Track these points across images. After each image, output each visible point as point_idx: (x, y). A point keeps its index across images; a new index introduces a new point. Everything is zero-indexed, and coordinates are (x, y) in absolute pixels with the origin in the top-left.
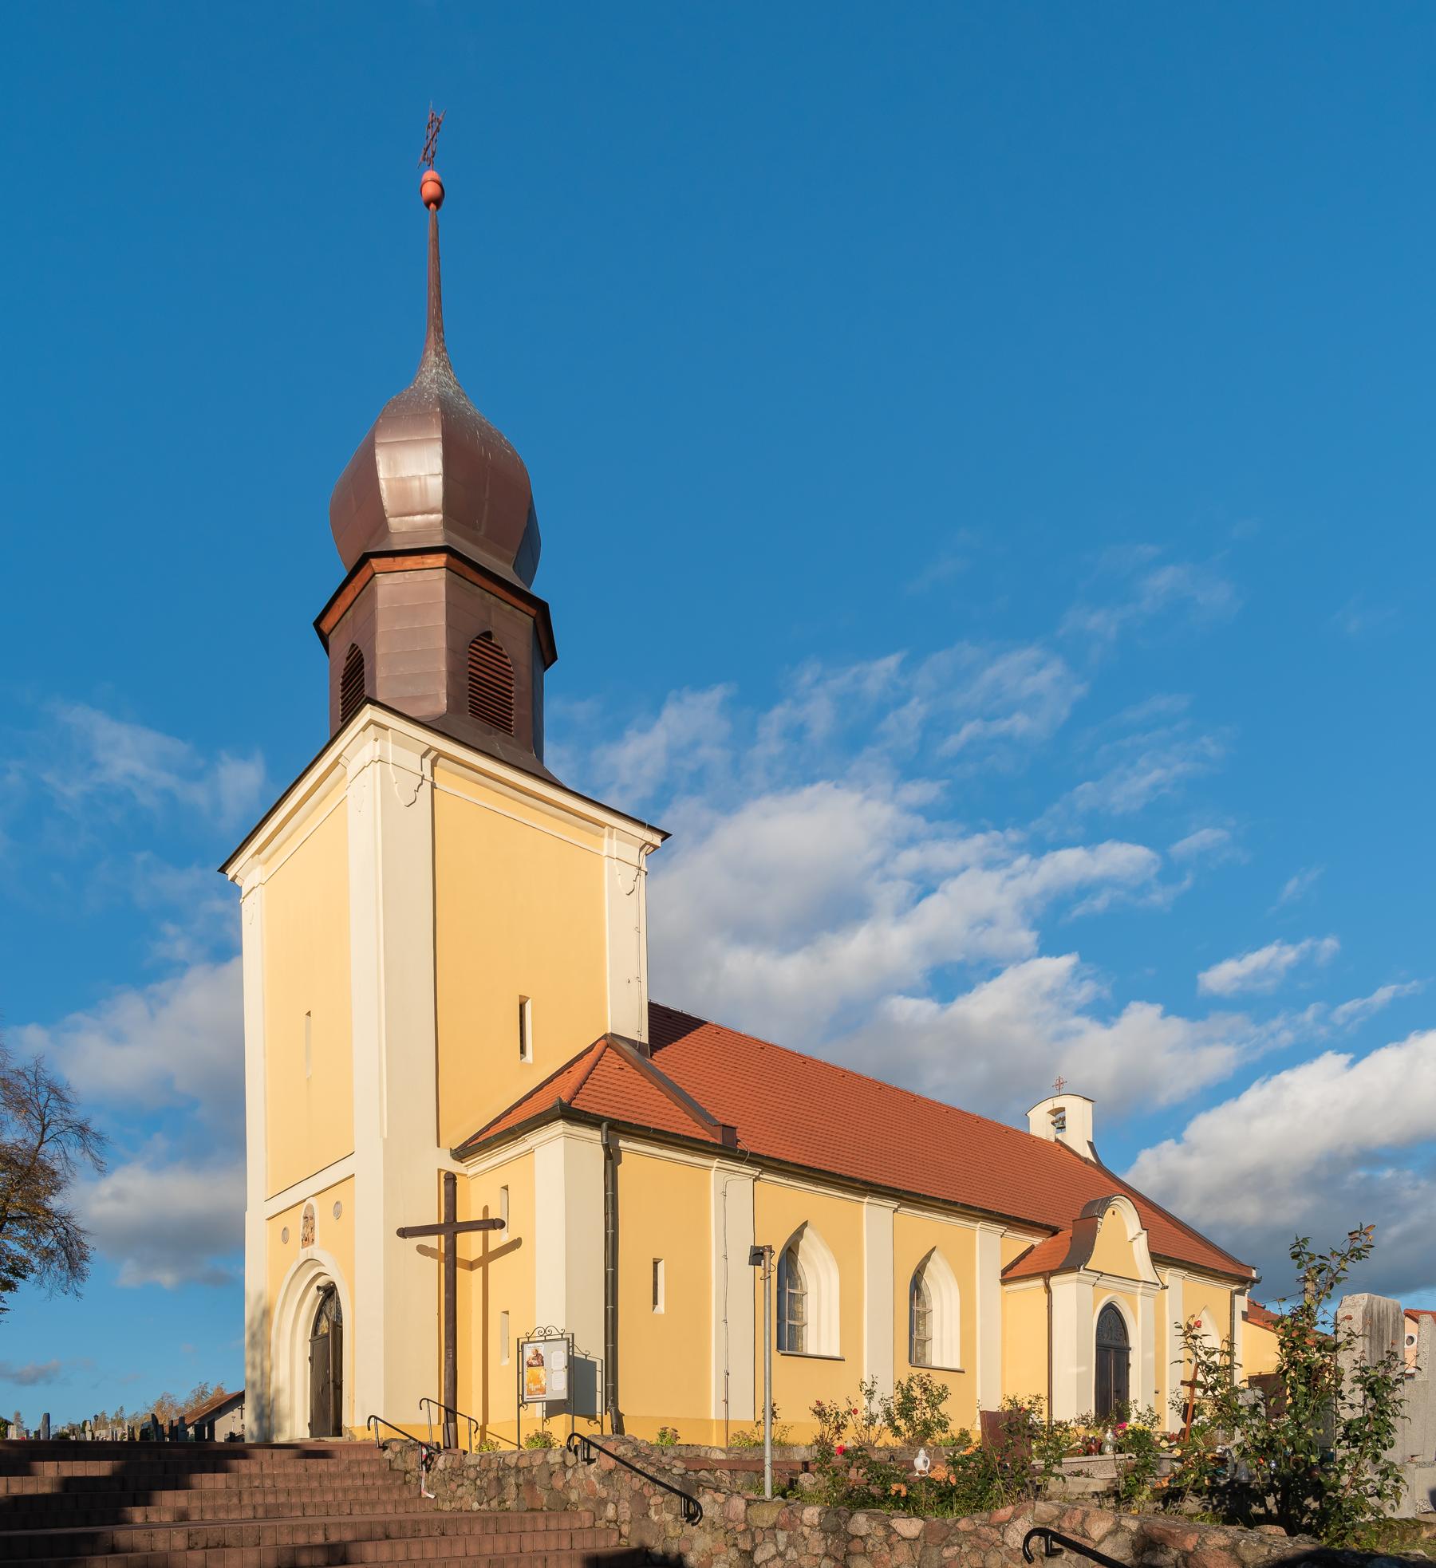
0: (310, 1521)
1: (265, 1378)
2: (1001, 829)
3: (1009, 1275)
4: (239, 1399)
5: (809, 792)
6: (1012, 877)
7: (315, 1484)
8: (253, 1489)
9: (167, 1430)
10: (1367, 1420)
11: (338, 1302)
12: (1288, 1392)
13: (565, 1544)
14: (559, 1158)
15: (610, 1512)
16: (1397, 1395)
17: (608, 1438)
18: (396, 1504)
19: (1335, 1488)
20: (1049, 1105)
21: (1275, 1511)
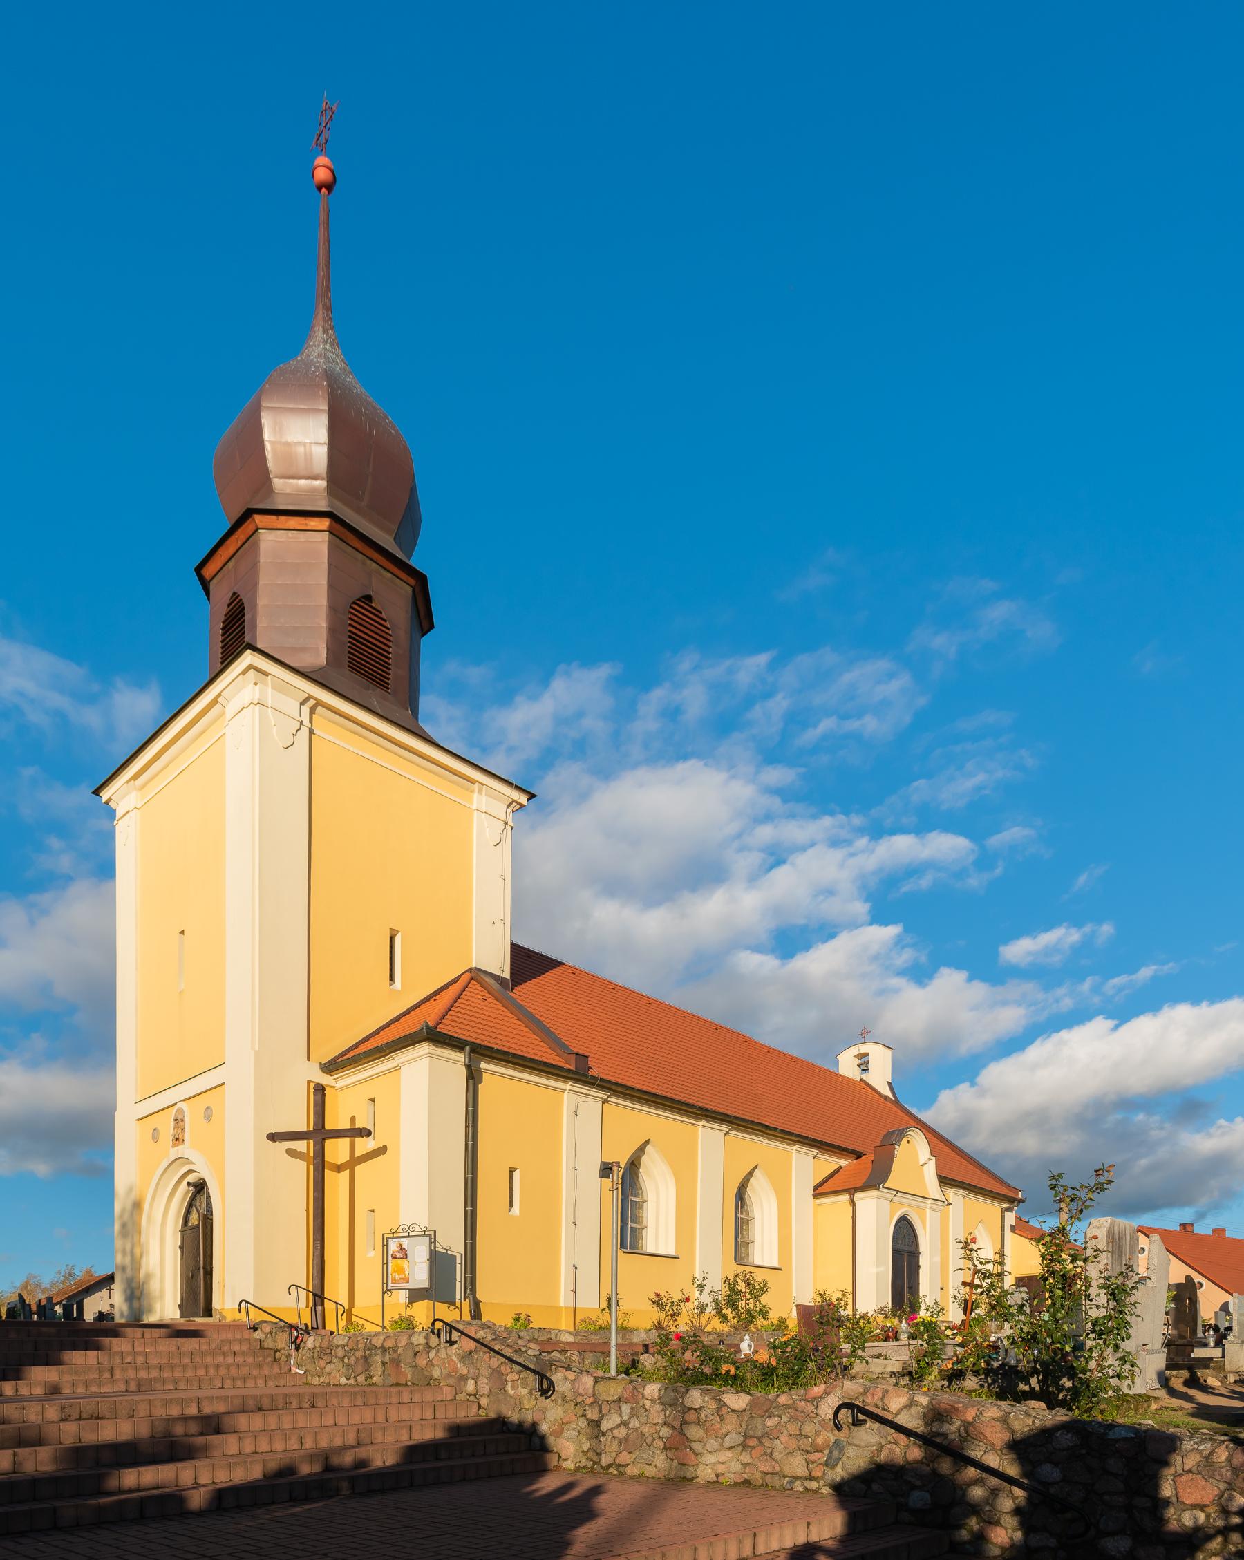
0: (183, 1395)
1: (136, 1264)
2: (847, 814)
3: (820, 1191)
4: (110, 1279)
5: (682, 768)
6: (852, 855)
7: (186, 1361)
8: (125, 1366)
9: (34, 1308)
10: (1109, 1318)
11: (208, 1197)
12: (1047, 1295)
13: (429, 1414)
14: (424, 1076)
15: (470, 1386)
16: (1133, 1299)
17: (469, 1324)
18: (266, 1378)
19: (1084, 1371)
20: (855, 1050)
21: (1037, 1388)
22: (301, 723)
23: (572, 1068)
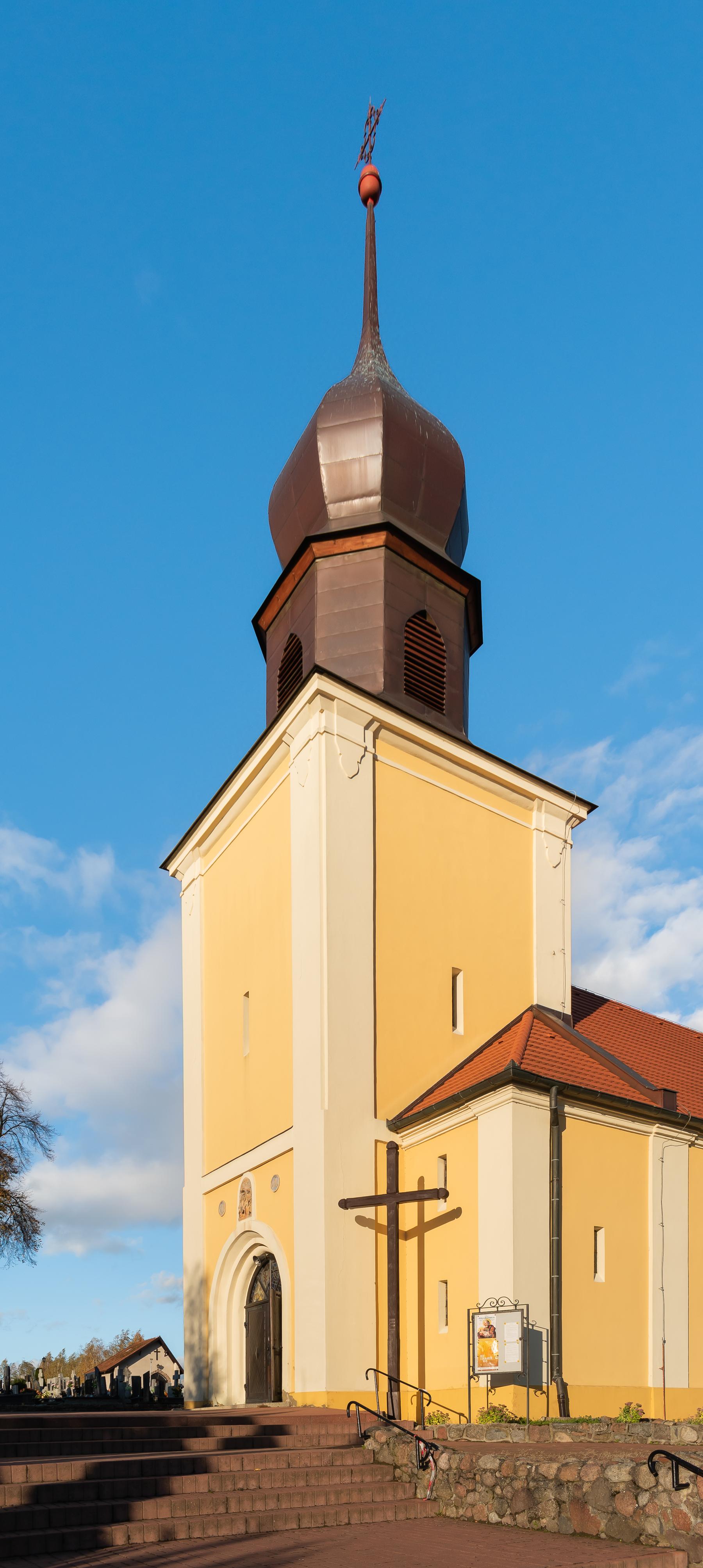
11: (276, 1271)
14: (506, 1123)
22: (366, 749)
23: (660, 1105)
